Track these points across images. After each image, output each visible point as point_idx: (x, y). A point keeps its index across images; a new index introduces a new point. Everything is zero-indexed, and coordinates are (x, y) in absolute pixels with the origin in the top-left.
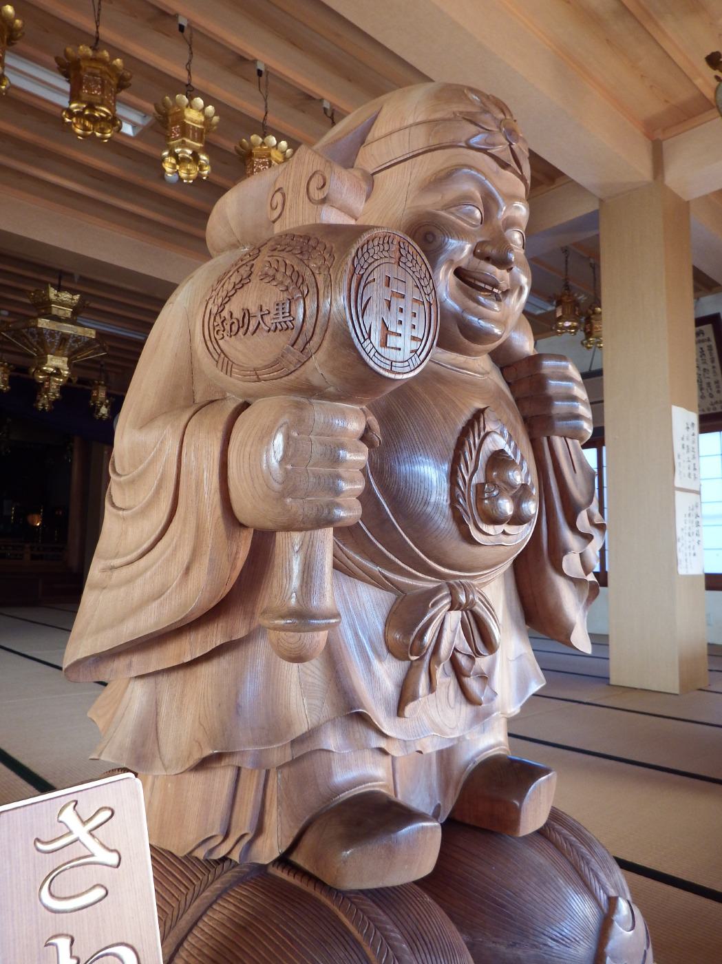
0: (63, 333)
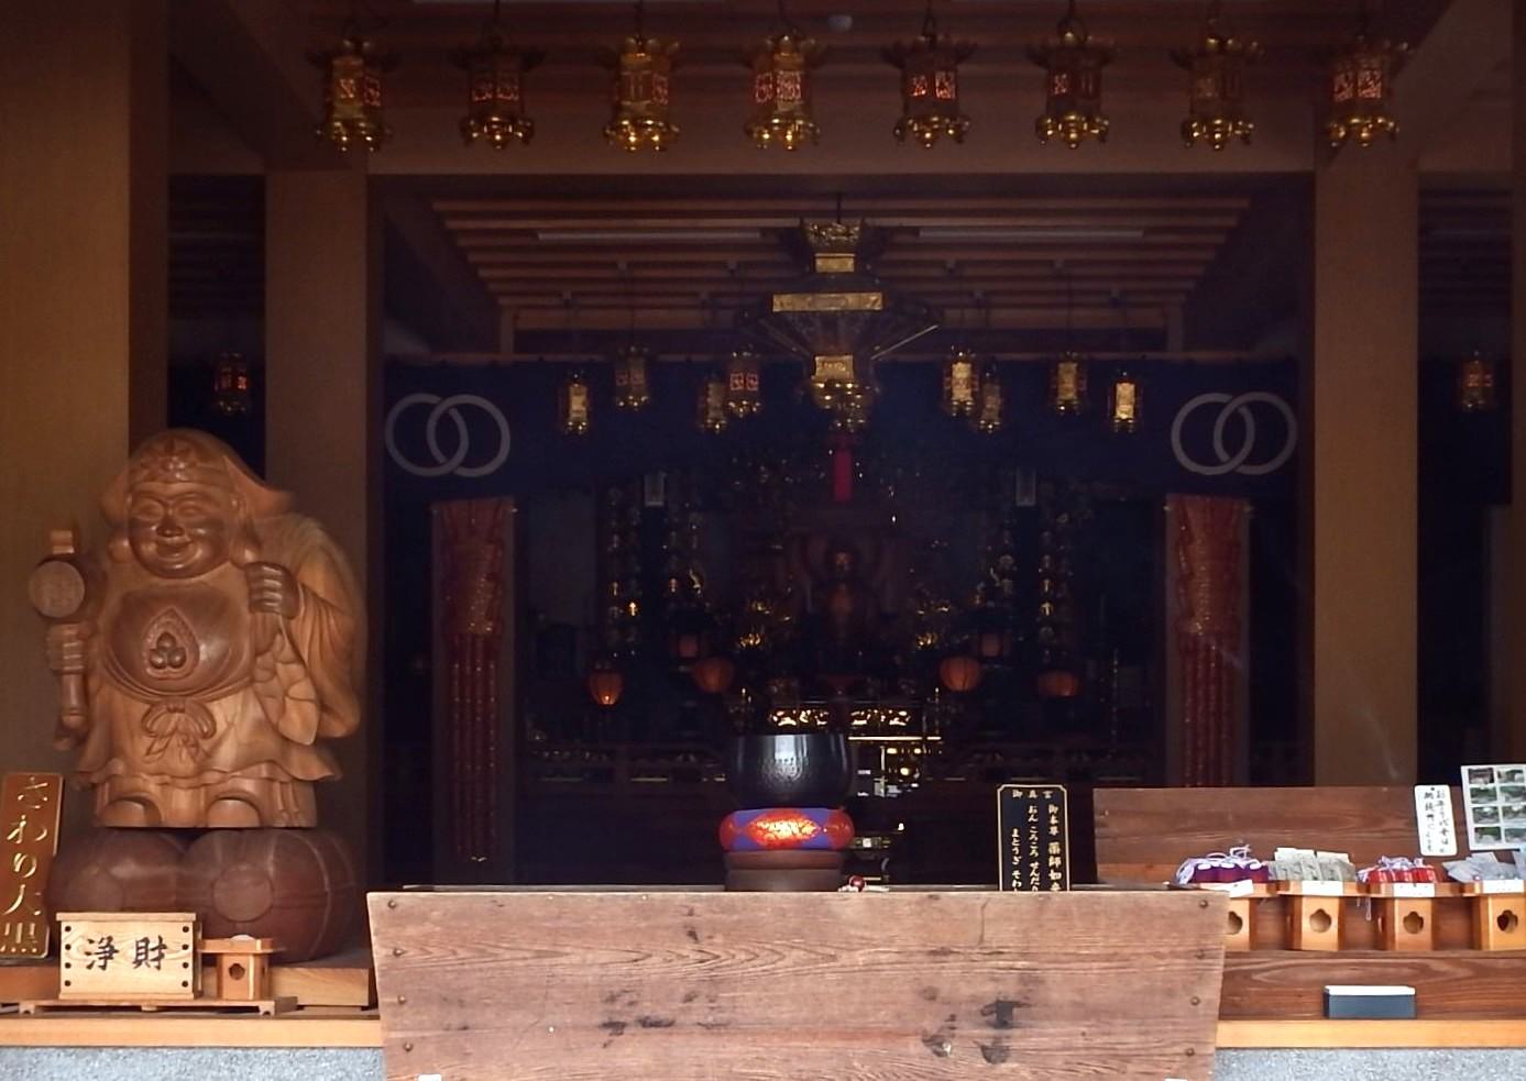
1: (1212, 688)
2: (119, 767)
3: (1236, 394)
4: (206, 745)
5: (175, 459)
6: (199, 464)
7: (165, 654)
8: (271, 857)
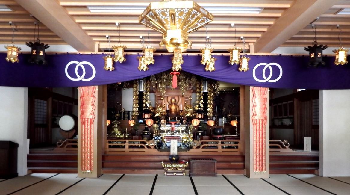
3: (268, 63)
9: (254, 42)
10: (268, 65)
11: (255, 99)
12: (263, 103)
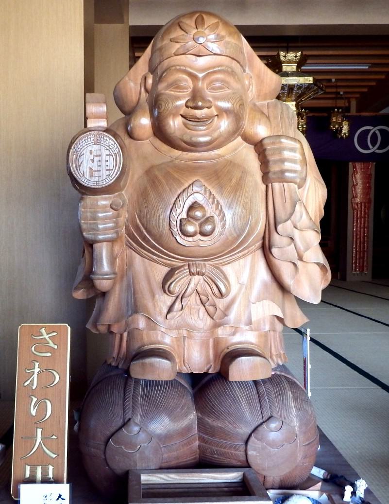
0: (289, 85)
1: (362, 220)
2: (142, 323)
3: (375, 127)
4: (221, 303)
5: (207, 32)
6: (228, 39)
7: (197, 224)
8: (294, 413)
9: (356, 98)
10: (373, 130)
11: (356, 176)
12: (367, 181)
